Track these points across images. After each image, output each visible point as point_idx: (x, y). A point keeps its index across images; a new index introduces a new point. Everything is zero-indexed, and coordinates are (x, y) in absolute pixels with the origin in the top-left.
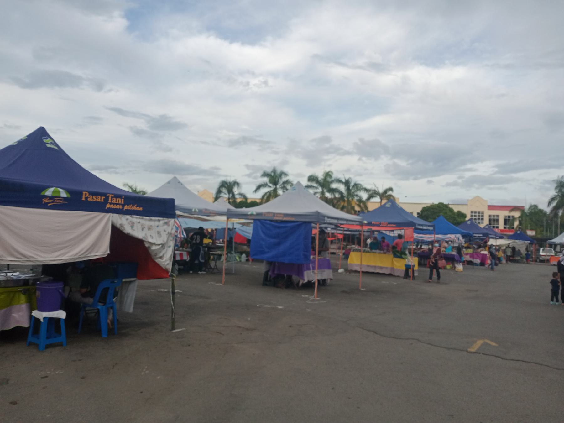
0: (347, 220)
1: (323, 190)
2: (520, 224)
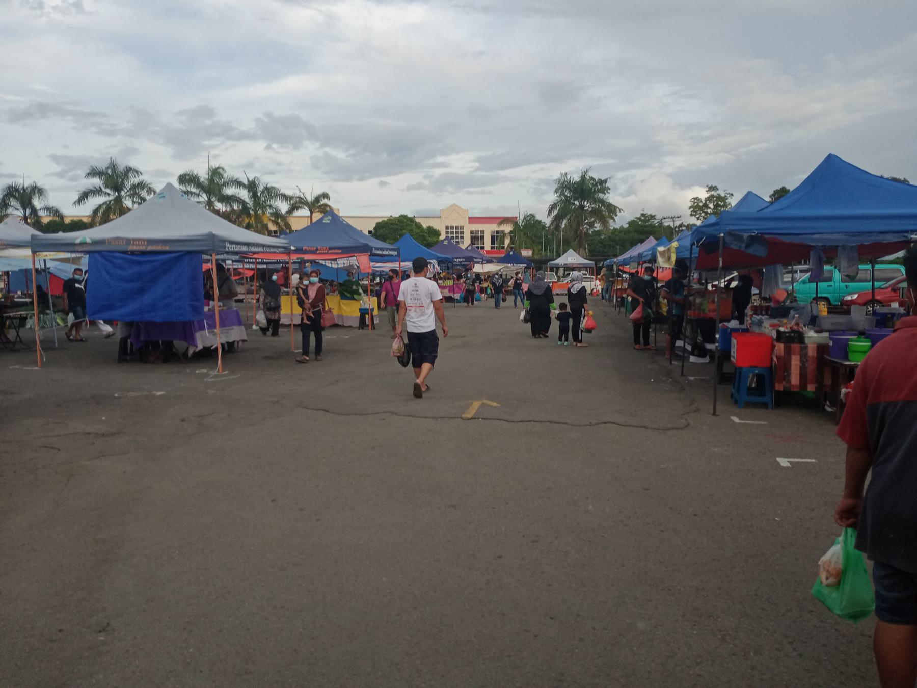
0: (264, 246)
1: (209, 199)
2: (512, 241)
